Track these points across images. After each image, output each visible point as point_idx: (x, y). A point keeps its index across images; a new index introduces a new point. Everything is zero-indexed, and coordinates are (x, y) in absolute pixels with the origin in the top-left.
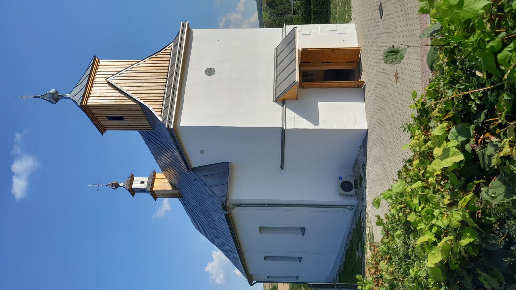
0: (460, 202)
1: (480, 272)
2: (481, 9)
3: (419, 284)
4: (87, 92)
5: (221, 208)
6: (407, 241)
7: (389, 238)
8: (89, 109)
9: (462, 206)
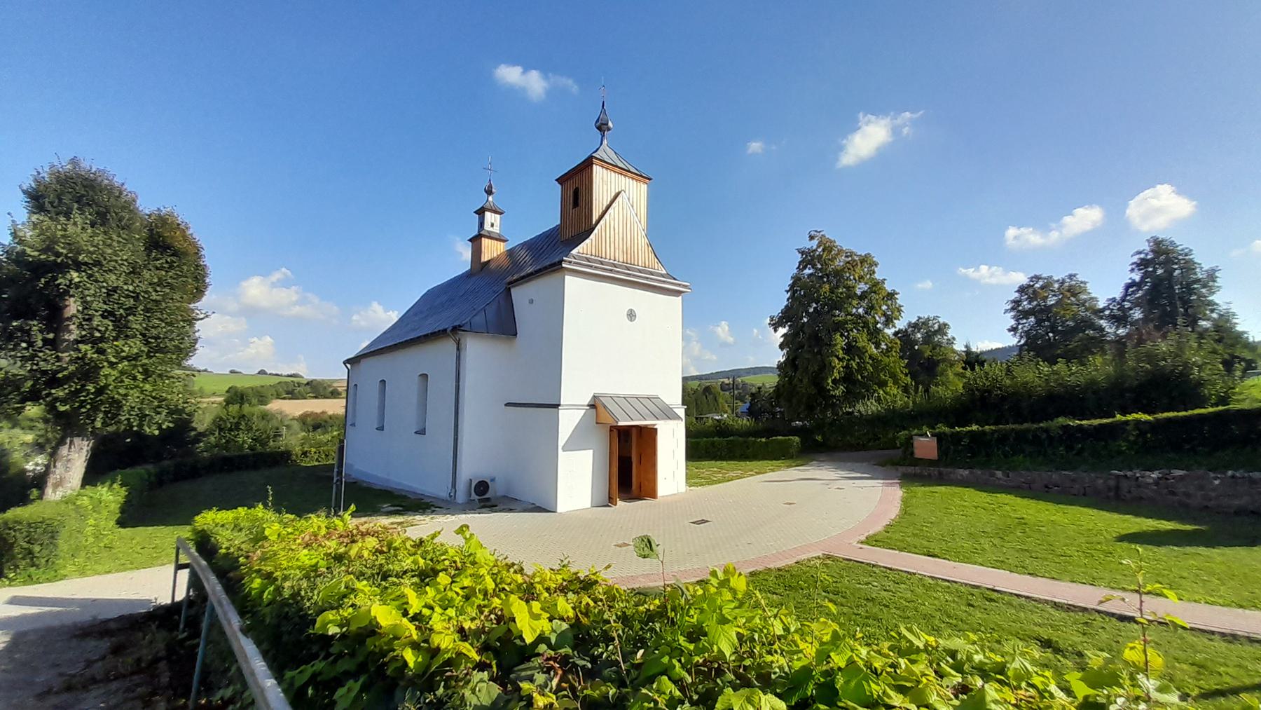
0: (467, 645)
1: (362, 680)
2: (719, 648)
3: (345, 596)
4: (606, 164)
5: (457, 324)
6: (409, 574)
7: (411, 549)
8: (587, 166)
9: (461, 648)
